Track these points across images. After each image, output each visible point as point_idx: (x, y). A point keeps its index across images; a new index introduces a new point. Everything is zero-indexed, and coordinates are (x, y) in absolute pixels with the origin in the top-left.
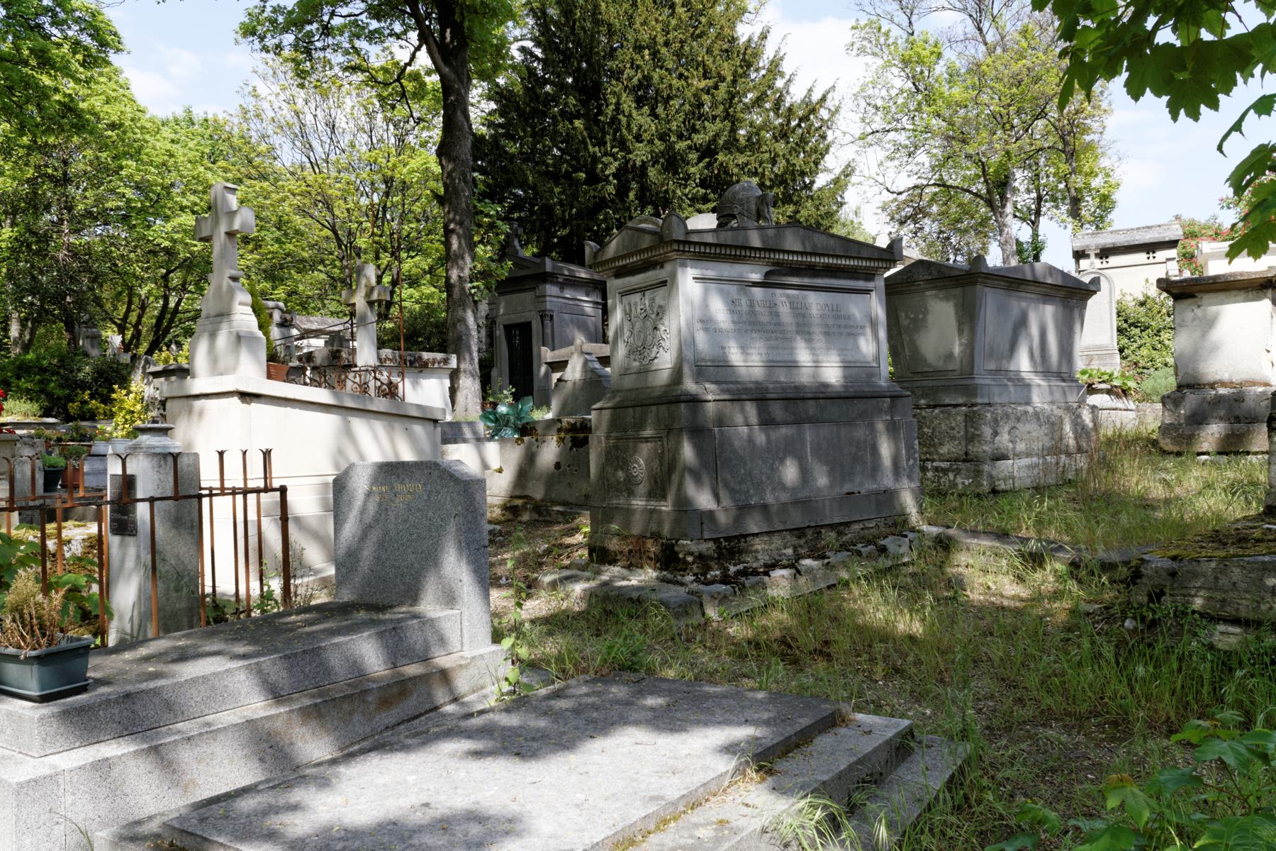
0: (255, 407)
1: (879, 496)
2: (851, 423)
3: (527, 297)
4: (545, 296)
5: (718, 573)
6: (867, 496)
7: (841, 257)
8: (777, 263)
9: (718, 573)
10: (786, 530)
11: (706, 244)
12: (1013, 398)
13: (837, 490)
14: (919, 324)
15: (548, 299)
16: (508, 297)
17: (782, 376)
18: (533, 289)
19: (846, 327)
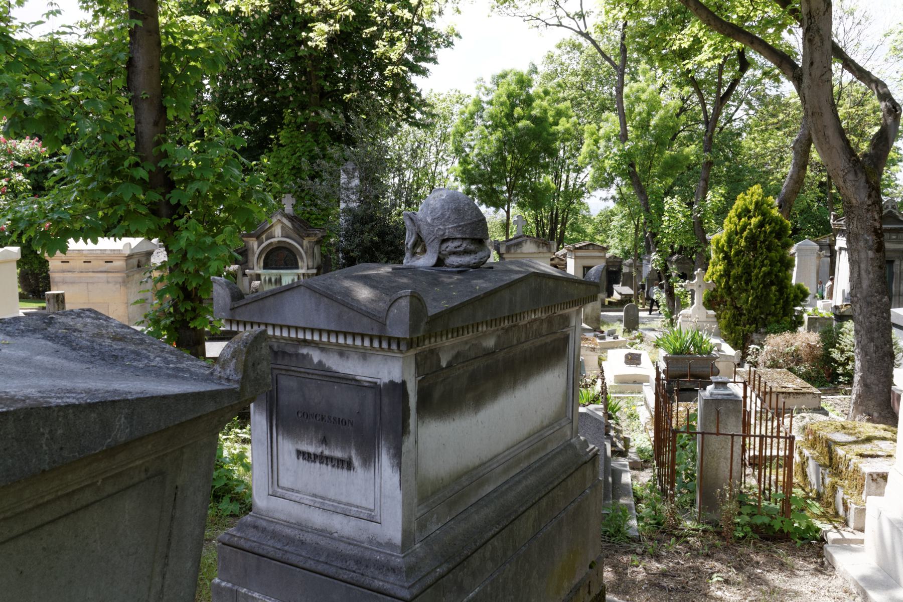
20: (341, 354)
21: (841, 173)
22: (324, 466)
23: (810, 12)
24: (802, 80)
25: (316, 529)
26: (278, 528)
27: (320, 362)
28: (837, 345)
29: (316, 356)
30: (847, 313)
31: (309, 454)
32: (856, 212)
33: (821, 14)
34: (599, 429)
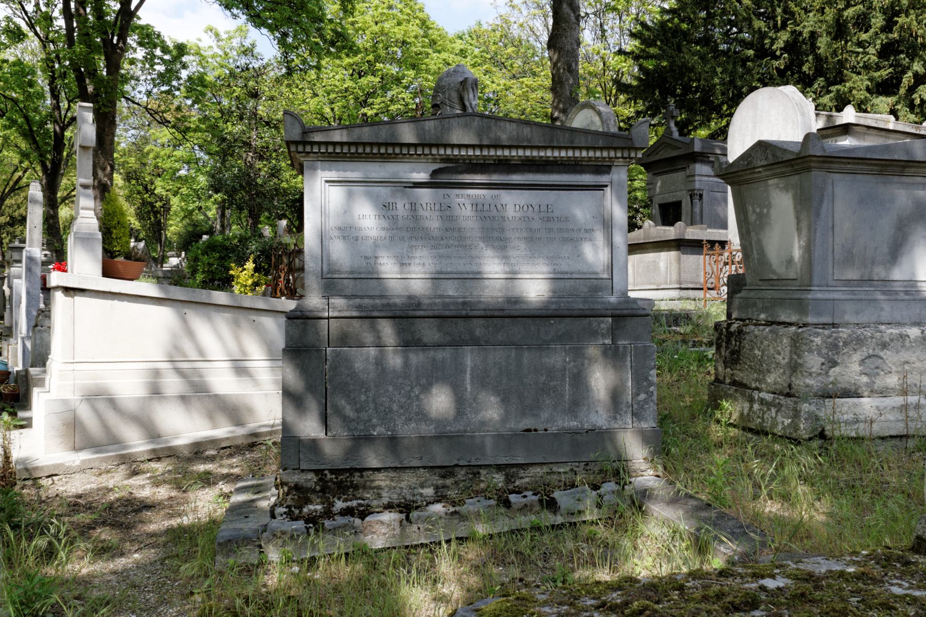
0: (79, 299)
1: (579, 437)
2: (542, 347)
3: (679, 176)
4: (694, 176)
5: (319, 507)
6: (555, 435)
7: (545, 148)
8: (447, 159)
9: (319, 507)
10: (424, 468)
11: (335, 144)
12: (885, 316)
13: (512, 425)
14: (763, 220)
15: (697, 178)
16: (664, 177)
17: (451, 290)
18: (684, 169)
19: (560, 230)
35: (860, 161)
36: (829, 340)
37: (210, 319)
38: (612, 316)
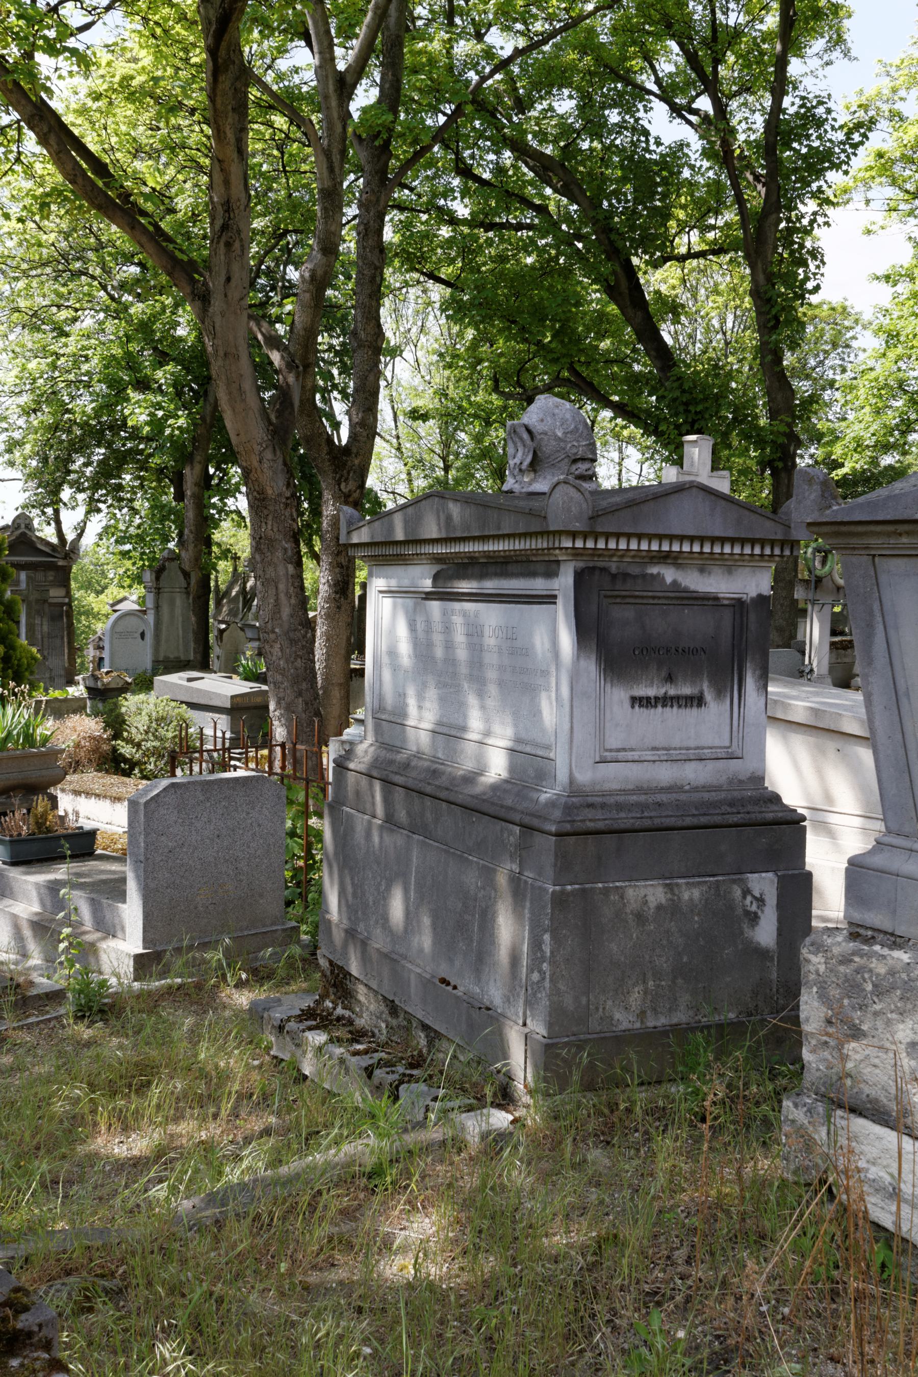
20: (702, 570)
21: (257, 448)
22: (668, 709)
23: (228, 201)
24: (209, 302)
25: (662, 788)
26: (621, 799)
27: (675, 582)
28: (125, 734)
29: (669, 574)
30: (113, 686)
31: (648, 699)
32: (271, 508)
33: (242, 207)
34: (279, 798)
35: (890, 528)
36: (842, 969)
37: (785, 738)
38: (521, 825)
